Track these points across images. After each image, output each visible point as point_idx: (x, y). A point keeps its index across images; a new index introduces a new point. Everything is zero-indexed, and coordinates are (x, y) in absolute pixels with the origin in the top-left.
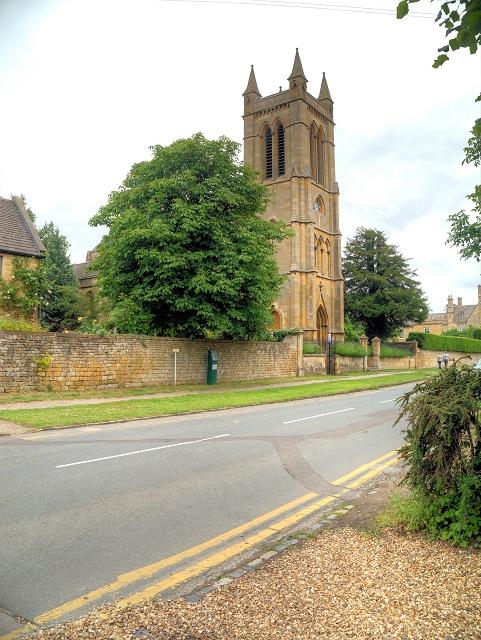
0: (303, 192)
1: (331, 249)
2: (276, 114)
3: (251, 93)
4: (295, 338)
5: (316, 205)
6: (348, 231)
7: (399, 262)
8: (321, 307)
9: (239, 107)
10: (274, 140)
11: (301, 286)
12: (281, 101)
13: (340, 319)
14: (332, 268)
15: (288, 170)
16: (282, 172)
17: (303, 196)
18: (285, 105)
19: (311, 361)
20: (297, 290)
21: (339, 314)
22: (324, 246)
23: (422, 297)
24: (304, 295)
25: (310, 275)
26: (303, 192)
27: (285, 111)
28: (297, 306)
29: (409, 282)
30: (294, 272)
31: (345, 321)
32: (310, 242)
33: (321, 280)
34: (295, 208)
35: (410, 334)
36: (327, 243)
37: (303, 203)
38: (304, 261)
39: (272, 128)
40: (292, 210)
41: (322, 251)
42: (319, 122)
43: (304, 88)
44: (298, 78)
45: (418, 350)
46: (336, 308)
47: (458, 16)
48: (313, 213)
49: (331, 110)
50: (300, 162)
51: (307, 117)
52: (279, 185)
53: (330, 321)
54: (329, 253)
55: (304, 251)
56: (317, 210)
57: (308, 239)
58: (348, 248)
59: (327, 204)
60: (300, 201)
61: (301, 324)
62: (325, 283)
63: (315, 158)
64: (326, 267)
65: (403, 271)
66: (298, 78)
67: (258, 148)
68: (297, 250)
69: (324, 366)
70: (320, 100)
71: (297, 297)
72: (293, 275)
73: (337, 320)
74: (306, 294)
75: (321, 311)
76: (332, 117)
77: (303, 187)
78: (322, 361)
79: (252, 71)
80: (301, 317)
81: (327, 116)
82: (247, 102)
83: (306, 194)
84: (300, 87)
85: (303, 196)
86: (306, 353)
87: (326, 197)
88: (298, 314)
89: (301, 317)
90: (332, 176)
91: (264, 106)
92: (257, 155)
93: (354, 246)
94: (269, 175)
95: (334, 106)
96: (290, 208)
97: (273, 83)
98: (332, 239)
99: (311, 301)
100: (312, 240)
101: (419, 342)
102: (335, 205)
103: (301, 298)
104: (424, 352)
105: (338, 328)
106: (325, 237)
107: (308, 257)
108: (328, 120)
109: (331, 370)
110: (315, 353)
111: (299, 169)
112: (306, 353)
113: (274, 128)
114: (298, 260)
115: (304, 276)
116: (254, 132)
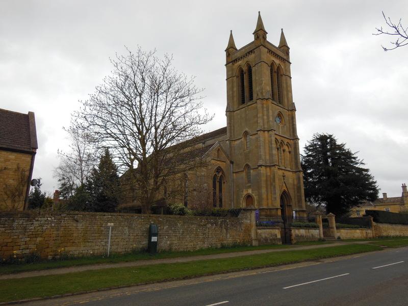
0: (265, 109)
1: (292, 149)
2: (246, 59)
3: (231, 49)
4: (248, 214)
5: (278, 119)
6: (306, 133)
7: (348, 155)
8: (284, 191)
9: (223, 59)
10: (246, 76)
11: (267, 176)
12: (250, 50)
13: (301, 199)
14: (293, 163)
15: (255, 96)
16: (251, 98)
17: (265, 113)
18: (251, 51)
19: (265, 233)
20: (264, 179)
21: (301, 196)
22: (286, 148)
23: (371, 180)
24: (269, 183)
25: (273, 168)
26: (265, 109)
27: (252, 56)
28: (264, 190)
29: (360, 170)
30: (261, 166)
31: (306, 201)
32: (272, 144)
33: (283, 171)
34: (260, 121)
35: (367, 211)
36: (288, 145)
37: (265, 117)
38: (268, 157)
39: (244, 69)
40: (258, 123)
41: (284, 151)
42: (277, 62)
43: (265, 38)
44: (260, 32)
45: (374, 223)
46: (298, 192)
47: (374, 221)
48: (275, 123)
49: (287, 54)
50: (262, 89)
51: (267, 57)
52: (249, 107)
53: (294, 202)
54: (290, 152)
55: (267, 151)
56: (278, 122)
57: (270, 142)
58: (306, 148)
59: (287, 118)
60: (263, 115)
61: (268, 205)
62: (287, 173)
63: (276, 86)
64: (288, 162)
65: (352, 162)
66: (260, 32)
67: (235, 84)
68: (262, 150)
69: (279, 236)
70: (280, 47)
71: (263, 184)
72: (260, 168)
73: (299, 201)
74: (271, 181)
75: (285, 196)
76: (289, 58)
77: (265, 106)
78: (277, 233)
79: (231, 35)
80: (267, 199)
81: (285, 57)
82: (228, 55)
83: (268, 110)
84: (261, 37)
85: (265, 113)
86: (260, 225)
87: (285, 113)
88: (264, 196)
89: (267, 199)
90: (290, 98)
91: (238, 55)
92: (235, 89)
93: (311, 148)
94: (243, 102)
95: (290, 51)
96: (257, 122)
97: (244, 40)
98: (291, 142)
99: (275, 187)
100: (274, 142)
101: (376, 217)
102: (293, 119)
103: (267, 184)
104: (381, 225)
105: (301, 207)
106: (286, 141)
107: (271, 155)
108: (286, 61)
109: (287, 239)
110: (272, 225)
111: (262, 93)
112: (260, 225)
113: (245, 69)
114: (263, 157)
115: (268, 169)
116: (232, 74)
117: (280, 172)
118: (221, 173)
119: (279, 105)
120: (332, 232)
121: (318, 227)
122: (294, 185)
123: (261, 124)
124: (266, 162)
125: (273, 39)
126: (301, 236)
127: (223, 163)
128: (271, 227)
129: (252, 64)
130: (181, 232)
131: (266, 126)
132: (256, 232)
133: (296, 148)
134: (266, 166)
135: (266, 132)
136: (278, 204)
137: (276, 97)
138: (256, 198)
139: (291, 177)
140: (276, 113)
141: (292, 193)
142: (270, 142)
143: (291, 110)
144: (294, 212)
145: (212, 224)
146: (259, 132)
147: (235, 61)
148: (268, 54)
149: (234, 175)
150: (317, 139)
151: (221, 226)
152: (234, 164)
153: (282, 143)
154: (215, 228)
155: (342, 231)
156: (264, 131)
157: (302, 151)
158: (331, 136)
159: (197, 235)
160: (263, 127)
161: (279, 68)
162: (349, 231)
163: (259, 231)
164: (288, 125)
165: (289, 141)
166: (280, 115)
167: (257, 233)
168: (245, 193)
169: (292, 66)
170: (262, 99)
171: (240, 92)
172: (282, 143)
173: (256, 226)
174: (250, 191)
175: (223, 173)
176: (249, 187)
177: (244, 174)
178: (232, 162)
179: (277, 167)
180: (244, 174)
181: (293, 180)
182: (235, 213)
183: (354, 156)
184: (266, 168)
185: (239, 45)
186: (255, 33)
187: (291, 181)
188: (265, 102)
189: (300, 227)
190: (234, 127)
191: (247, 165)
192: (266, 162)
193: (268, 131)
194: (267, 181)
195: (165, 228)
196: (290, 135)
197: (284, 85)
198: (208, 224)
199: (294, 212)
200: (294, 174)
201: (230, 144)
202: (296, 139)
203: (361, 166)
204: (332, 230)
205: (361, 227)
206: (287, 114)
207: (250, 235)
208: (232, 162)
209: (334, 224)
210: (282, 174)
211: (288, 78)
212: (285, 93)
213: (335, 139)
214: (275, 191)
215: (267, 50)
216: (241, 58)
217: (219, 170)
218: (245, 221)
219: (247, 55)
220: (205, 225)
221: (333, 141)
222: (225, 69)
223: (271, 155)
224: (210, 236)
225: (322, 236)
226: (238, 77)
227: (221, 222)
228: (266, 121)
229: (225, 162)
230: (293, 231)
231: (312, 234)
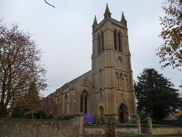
4: (78, 118)
8: (122, 104)
11: (109, 94)
12: (103, 23)
17: (109, 57)
20: (107, 96)
22: (124, 77)
24: (110, 98)
33: (122, 91)
34: (106, 62)
36: (125, 75)
37: (109, 60)
38: (110, 83)
42: (118, 29)
44: (107, 14)
49: (126, 24)
54: (127, 80)
61: (110, 112)
62: (124, 93)
66: (107, 14)
75: (122, 107)
81: (124, 26)
82: (93, 28)
85: (109, 57)
87: (124, 58)
92: (96, 46)
103: (109, 100)
105: (134, 113)
106: (124, 73)
111: (107, 46)
114: (107, 83)
115: (110, 90)
116: (95, 38)
117: (119, 92)
118: (86, 94)
119: (120, 53)
120: (150, 130)
121: (137, 127)
122: (130, 100)
123: (107, 64)
124: (109, 86)
125: (116, 17)
126: (122, 133)
127: (88, 87)
128: (163, 128)
129: (103, 31)
130: (18, 130)
131: (109, 65)
132: (84, 130)
133: (131, 77)
134: (109, 88)
135: (109, 68)
136: (116, 111)
137: (118, 48)
138: (104, 108)
139: (127, 96)
140: (117, 57)
141: (128, 105)
142: (112, 74)
143: (127, 56)
144: (130, 117)
145: (46, 125)
146: (105, 69)
147: (97, 30)
148: (112, 25)
149: (95, 94)
150: (146, 71)
151: (53, 126)
152: (95, 88)
153: (121, 75)
154: (48, 127)
155: (158, 129)
156: (108, 68)
157: (136, 80)
158: (153, 69)
159: (32, 131)
160: (107, 66)
161: (120, 32)
162: (164, 129)
163: (86, 129)
164: (126, 64)
165: (126, 73)
166: (120, 58)
167: (84, 131)
168: (99, 105)
169: (128, 31)
170: (107, 50)
171: (121, 46)
172: (121, 75)
173: (84, 126)
174: (102, 104)
175: (87, 93)
176: (102, 101)
177: (99, 94)
178: (94, 87)
179: (115, 89)
180: (99, 94)
181: (129, 97)
182: (68, 118)
183: (169, 81)
184: (109, 90)
185: (99, 22)
186: (105, 15)
187: (127, 97)
188: (109, 51)
189: (122, 126)
190: (95, 67)
191: (101, 89)
192: (109, 86)
193: (111, 67)
194: (109, 97)
195: (4, 127)
196: (127, 70)
197: (123, 42)
198: (42, 124)
199: (130, 117)
200: (130, 93)
201: (93, 76)
202: (131, 72)
203: (174, 88)
204: (149, 128)
205: (174, 127)
206: (125, 57)
207: (78, 132)
208: (94, 87)
209: (151, 124)
210: (121, 93)
211: (126, 38)
212: (124, 46)
213: (156, 71)
214: (114, 103)
215: (111, 23)
216: (99, 29)
217: (85, 91)
218: (74, 122)
219: (101, 27)
220: (40, 125)
221: (156, 73)
222: (92, 35)
223: (112, 81)
224: (43, 133)
225: (140, 133)
226: (97, 39)
227: (54, 124)
228: (109, 62)
229: (89, 87)
230: (115, 129)
231: (132, 132)
